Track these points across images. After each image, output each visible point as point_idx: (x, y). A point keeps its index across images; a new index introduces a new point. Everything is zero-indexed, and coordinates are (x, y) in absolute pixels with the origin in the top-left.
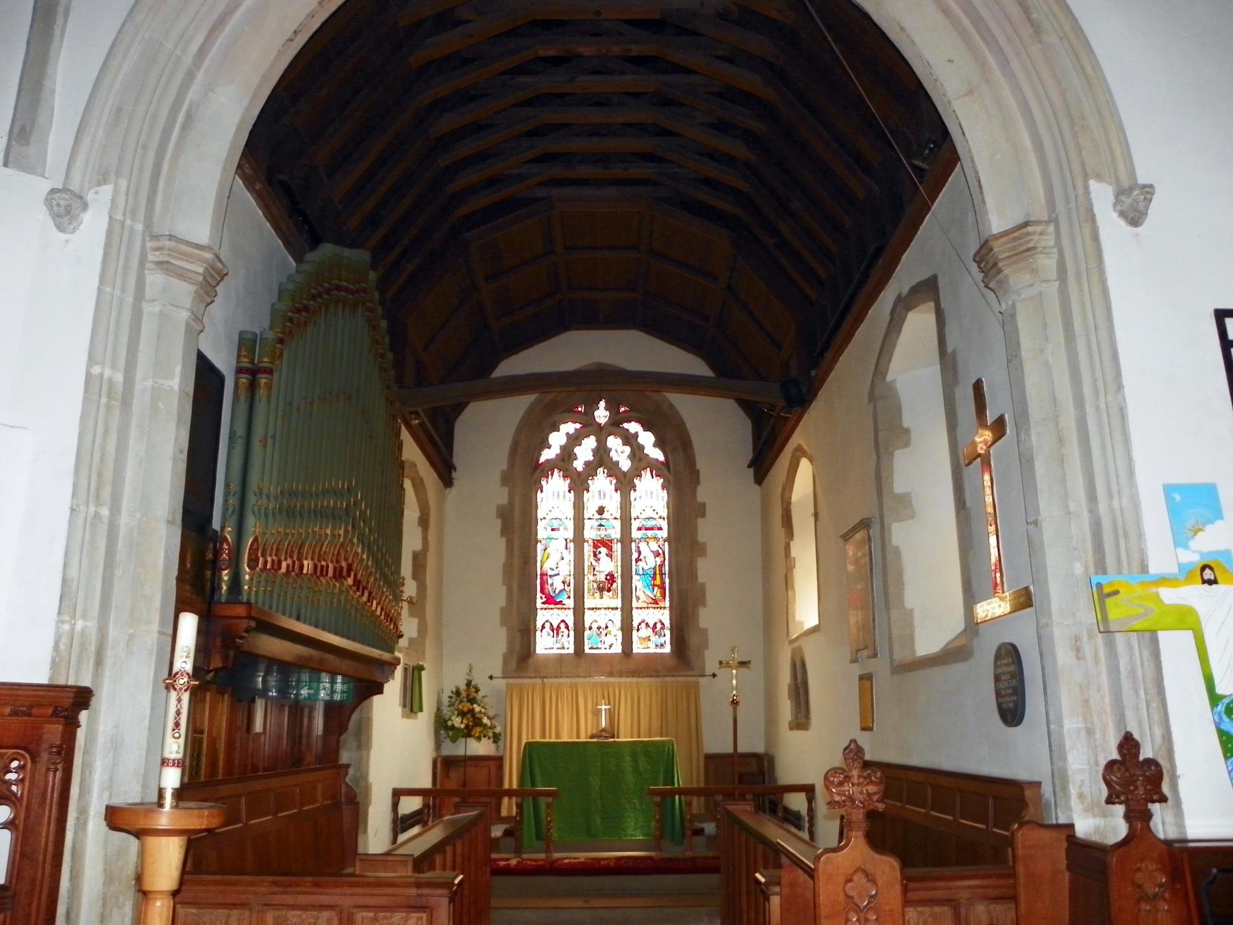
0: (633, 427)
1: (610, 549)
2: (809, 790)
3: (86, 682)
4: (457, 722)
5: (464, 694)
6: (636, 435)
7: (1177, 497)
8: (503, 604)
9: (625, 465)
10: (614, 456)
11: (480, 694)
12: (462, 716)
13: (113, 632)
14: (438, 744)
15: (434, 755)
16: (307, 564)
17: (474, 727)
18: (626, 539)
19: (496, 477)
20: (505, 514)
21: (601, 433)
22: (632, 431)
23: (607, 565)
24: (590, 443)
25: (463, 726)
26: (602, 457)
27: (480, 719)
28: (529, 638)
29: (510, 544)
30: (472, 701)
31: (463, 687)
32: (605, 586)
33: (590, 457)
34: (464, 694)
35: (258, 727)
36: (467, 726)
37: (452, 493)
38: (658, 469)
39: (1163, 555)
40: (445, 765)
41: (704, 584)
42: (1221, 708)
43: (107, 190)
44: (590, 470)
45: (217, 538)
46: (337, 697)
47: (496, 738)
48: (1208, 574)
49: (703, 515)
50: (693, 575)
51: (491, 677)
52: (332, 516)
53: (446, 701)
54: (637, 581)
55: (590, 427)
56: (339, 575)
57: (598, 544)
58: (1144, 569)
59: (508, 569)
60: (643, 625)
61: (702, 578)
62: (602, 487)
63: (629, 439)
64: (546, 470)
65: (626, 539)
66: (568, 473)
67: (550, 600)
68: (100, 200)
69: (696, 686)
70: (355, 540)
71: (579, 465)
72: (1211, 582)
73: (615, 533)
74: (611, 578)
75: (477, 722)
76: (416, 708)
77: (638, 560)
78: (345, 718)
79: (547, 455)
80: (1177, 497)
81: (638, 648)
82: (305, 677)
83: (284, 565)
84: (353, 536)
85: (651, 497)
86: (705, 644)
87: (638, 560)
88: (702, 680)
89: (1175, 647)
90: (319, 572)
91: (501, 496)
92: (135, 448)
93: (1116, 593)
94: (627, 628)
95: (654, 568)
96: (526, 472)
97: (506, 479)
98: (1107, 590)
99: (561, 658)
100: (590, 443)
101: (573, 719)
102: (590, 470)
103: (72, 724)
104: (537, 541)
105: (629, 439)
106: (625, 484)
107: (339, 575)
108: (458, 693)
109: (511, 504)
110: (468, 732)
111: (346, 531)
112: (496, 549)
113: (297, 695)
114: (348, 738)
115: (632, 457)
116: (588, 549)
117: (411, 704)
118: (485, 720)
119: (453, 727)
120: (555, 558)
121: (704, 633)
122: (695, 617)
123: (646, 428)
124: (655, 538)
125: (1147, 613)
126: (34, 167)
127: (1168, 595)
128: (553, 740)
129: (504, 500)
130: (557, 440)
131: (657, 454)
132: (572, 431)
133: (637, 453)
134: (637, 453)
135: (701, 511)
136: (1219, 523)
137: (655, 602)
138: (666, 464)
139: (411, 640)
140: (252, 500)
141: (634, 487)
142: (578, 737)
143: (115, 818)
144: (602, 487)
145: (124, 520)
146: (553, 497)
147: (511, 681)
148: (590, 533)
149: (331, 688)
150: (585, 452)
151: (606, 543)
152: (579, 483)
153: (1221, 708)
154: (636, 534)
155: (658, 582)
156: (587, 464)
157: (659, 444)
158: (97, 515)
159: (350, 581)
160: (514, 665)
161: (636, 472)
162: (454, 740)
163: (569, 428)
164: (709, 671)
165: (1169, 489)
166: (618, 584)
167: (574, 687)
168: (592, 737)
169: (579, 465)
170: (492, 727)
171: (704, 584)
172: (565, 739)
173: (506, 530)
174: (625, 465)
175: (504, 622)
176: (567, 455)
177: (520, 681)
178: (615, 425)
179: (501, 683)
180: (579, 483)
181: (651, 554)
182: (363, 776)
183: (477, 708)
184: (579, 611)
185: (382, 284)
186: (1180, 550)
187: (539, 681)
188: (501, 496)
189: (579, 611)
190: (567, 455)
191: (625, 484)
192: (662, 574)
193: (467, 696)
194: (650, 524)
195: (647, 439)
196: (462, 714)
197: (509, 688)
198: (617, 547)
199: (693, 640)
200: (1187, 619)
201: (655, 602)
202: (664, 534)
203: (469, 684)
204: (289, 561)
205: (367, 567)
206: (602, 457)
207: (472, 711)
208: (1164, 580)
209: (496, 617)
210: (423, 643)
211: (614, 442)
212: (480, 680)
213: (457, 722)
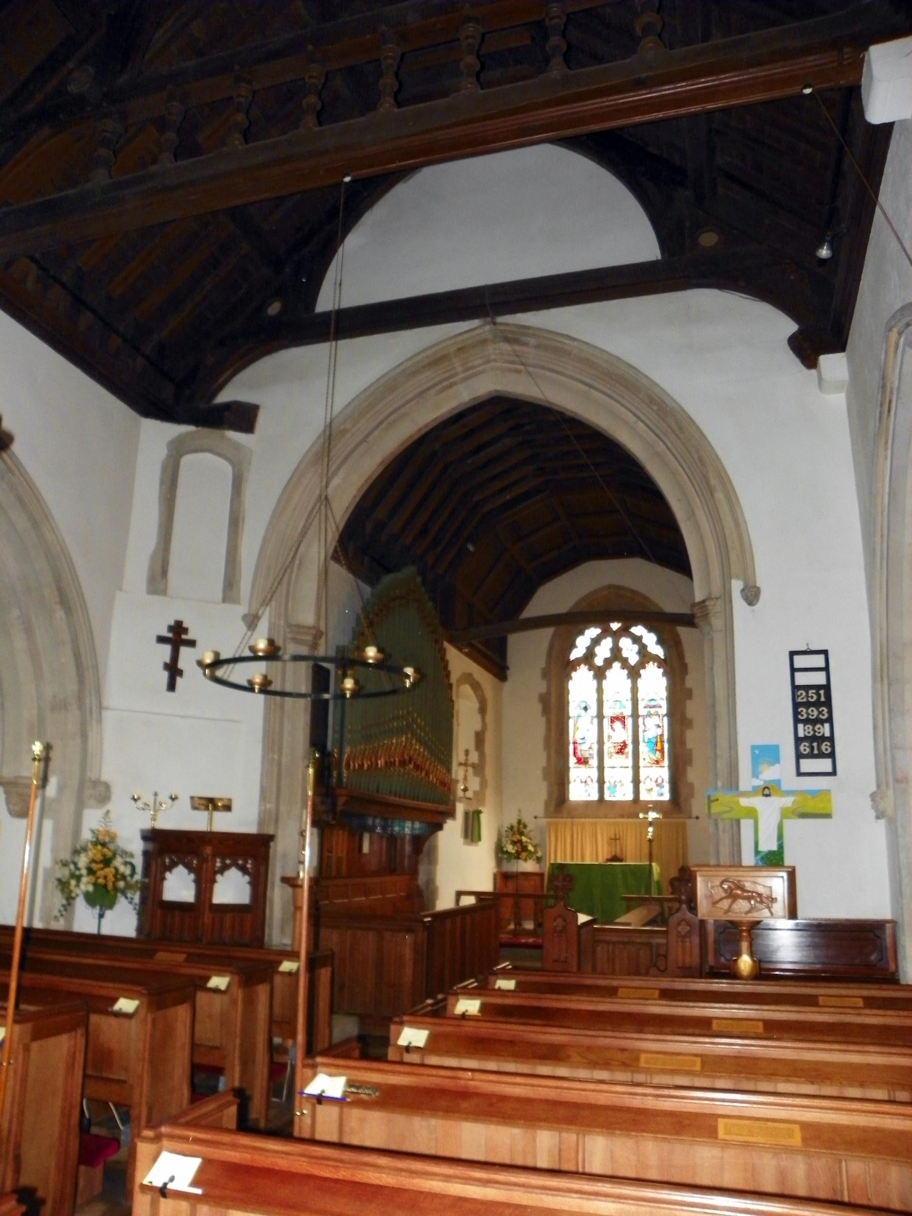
0: (638, 630)
1: (624, 723)
3: (271, 832)
4: (510, 848)
5: (515, 829)
6: (640, 638)
7: (757, 752)
8: (545, 765)
9: (634, 659)
10: (625, 654)
11: (529, 828)
12: (513, 843)
13: (282, 808)
14: (499, 862)
15: (495, 870)
16: (381, 763)
17: (522, 851)
18: (635, 715)
19: (538, 673)
20: (544, 700)
22: (638, 634)
23: (621, 734)
24: (607, 643)
25: (513, 851)
26: (616, 654)
27: (526, 847)
28: (564, 789)
29: (548, 722)
30: (521, 834)
31: (515, 824)
32: (621, 750)
33: (608, 655)
34: (515, 829)
35: (366, 848)
36: (517, 851)
37: (507, 686)
38: (661, 663)
39: (746, 781)
40: (503, 877)
41: (691, 750)
42: (759, 857)
44: (608, 663)
45: (330, 755)
46: (417, 832)
47: (539, 860)
48: (767, 791)
50: (683, 743)
51: (536, 817)
52: (399, 732)
53: (504, 833)
54: (643, 749)
55: (606, 632)
56: (403, 763)
57: (613, 720)
58: (737, 788)
59: (547, 740)
60: (648, 780)
62: (617, 675)
63: (637, 640)
64: (573, 666)
65: (635, 715)
66: (592, 667)
67: (582, 761)
69: (684, 825)
70: (414, 742)
71: (599, 661)
72: (767, 795)
73: (628, 711)
74: (624, 745)
75: (524, 848)
76: (819, 808)
77: (645, 731)
78: (422, 845)
79: (576, 654)
80: (757, 752)
83: (366, 766)
84: (412, 740)
85: (654, 683)
86: (691, 795)
87: (645, 731)
88: (688, 821)
89: (746, 826)
90: (389, 764)
91: (542, 687)
92: (287, 726)
93: (717, 800)
94: (636, 781)
95: (656, 737)
96: (560, 668)
97: (545, 674)
98: (712, 799)
99: (587, 804)
100: (607, 643)
101: (587, 849)
102: (608, 663)
103: (268, 847)
104: (569, 718)
105: (637, 640)
106: (634, 673)
107: (403, 763)
108: (512, 828)
109: (549, 692)
110: (517, 856)
111: (407, 738)
112: (539, 726)
113: (392, 830)
114: (423, 857)
115: (639, 653)
116: (606, 722)
117: (471, 833)
118: (530, 848)
119: (507, 852)
120: (582, 729)
121: (691, 785)
122: (684, 773)
123: (650, 629)
124: (658, 715)
125: (732, 809)
127: (744, 802)
128: (580, 863)
130: (582, 643)
132: (594, 636)
133: (643, 652)
134: (643, 652)
135: (689, 694)
136: (777, 765)
137: (657, 762)
138: (665, 661)
139: (476, 793)
140: (347, 736)
141: (640, 676)
142: (597, 860)
143: (285, 880)
144: (617, 675)
145: (284, 759)
146: (580, 684)
147: (549, 820)
148: (608, 712)
149: (409, 828)
150: (603, 651)
151: (621, 719)
152: (600, 674)
153: (759, 857)
154: (642, 711)
155: (659, 747)
156: (606, 660)
157: (660, 642)
158: (273, 759)
159: (411, 766)
160: (552, 808)
161: (642, 664)
162: (509, 860)
163: (593, 632)
164: (695, 814)
165: (754, 748)
166: (629, 749)
167: (595, 825)
168: (608, 860)
169: (599, 661)
170: (536, 852)
171: (691, 750)
172: (588, 861)
173: (546, 710)
174: (634, 659)
176: (589, 657)
177: (556, 820)
178: (625, 631)
179: (544, 821)
180: (600, 674)
181: (655, 726)
182: (431, 881)
183: (524, 839)
184: (601, 768)
185: (424, 583)
186: (754, 780)
187: (569, 820)
188: (542, 687)
189: (601, 768)
190: (589, 657)
191: (634, 673)
192: (662, 742)
193: (519, 829)
194: (653, 703)
195: (650, 639)
196: (514, 843)
197: (549, 824)
198: (629, 722)
199: (684, 791)
200: (752, 814)
201: (657, 762)
202: (664, 710)
203: (519, 822)
204: (369, 763)
205: (424, 755)
206: (616, 654)
207: (520, 841)
208: (745, 794)
209: (539, 773)
210: (484, 795)
211: (625, 643)
212: (527, 819)
213: (510, 848)
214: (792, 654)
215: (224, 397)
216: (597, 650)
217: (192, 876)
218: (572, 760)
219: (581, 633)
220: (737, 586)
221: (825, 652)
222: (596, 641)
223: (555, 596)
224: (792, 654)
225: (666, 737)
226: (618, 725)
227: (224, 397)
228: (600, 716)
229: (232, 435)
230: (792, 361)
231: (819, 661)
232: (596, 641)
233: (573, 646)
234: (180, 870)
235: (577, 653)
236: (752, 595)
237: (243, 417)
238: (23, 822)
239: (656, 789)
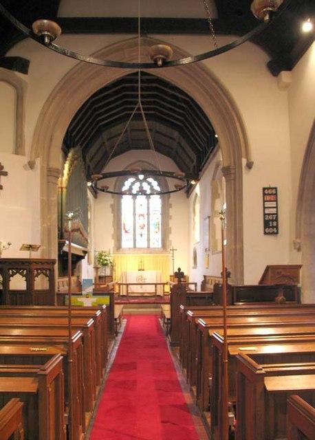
0: (150, 180)
2: (196, 284)
18: (148, 214)
21: (141, 181)
23: (143, 221)
43: (39, 159)
49: (171, 219)
54: (151, 227)
55: (138, 180)
59: (114, 222)
61: (170, 226)
63: (149, 184)
65: (148, 214)
68: (38, 162)
71: (134, 192)
81: (151, 246)
82: (195, 277)
100: (138, 184)
105: (149, 184)
116: (137, 216)
126: (23, 154)
129: (112, 202)
130: (128, 184)
131: (158, 189)
133: (152, 188)
134: (152, 188)
135: (170, 217)
150: (136, 188)
151: (143, 215)
157: (159, 185)
163: (131, 180)
169: (134, 192)
175: (113, 238)
176: (131, 188)
178: (145, 179)
190: (131, 188)
195: (155, 183)
198: (146, 217)
202: (154, 122)
209: (111, 238)
214: (264, 189)
215: (9, 54)
216: (133, 187)
217: (24, 278)
218: (123, 231)
219: (127, 180)
220: (244, 161)
221: (276, 188)
222: (133, 184)
223: (114, 165)
224: (264, 189)
225: (160, 223)
226: (142, 217)
227: (9, 54)
228: (134, 214)
229: (17, 73)
230: (268, 74)
231: (274, 192)
232: (133, 184)
233: (124, 185)
234: (18, 276)
235: (125, 188)
236: (249, 166)
237: (23, 66)
238: (100, 250)
239: (156, 242)
